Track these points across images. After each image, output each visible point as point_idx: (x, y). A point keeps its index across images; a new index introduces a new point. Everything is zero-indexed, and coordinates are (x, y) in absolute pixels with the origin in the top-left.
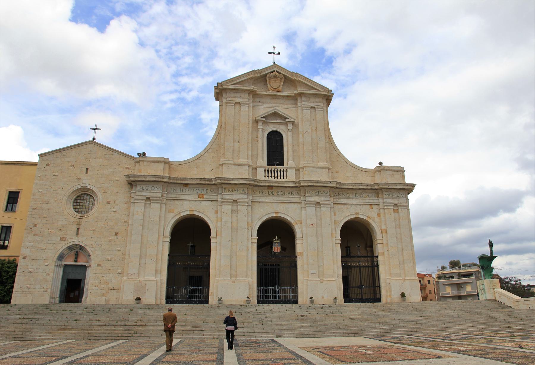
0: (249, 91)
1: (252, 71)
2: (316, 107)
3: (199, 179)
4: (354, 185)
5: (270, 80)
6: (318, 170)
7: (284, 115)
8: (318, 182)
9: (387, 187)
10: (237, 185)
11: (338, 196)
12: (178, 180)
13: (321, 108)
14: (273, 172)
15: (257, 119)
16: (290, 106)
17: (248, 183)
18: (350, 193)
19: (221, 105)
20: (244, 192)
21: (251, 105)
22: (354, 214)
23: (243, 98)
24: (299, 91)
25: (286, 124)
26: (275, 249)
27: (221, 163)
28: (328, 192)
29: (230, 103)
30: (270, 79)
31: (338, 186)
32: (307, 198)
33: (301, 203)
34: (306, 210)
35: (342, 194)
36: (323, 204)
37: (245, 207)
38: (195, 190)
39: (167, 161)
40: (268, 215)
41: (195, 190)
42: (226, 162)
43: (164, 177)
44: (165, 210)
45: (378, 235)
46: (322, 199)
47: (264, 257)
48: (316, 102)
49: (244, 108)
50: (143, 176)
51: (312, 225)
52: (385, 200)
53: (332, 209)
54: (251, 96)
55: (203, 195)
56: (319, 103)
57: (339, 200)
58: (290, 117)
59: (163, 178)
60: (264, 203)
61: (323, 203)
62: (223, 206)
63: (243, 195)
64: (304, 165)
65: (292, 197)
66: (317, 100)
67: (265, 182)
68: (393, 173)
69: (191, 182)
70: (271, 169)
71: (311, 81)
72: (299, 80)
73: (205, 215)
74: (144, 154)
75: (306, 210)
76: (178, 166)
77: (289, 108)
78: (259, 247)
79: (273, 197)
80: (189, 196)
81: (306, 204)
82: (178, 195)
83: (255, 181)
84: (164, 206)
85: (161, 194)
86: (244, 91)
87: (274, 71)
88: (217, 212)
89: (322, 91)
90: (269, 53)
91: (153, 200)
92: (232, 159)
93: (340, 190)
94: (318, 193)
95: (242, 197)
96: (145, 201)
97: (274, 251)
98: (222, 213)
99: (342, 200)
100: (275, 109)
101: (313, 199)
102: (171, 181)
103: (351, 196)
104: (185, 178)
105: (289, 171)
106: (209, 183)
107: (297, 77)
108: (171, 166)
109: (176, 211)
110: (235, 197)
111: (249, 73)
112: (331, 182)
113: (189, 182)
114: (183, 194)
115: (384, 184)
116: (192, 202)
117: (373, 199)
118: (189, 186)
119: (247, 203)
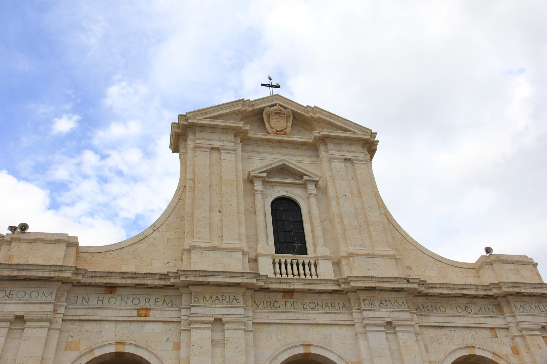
1: (239, 101)
3: (140, 276)
4: (451, 286)
5: (269, 118)
6: (378, 261)
7: (300, 170)
8: (385, 280)
9: (518, 290)
10: (222, 288)
11: (423, 311)
12: (95, 277)
13: (362, 161)
15: (251, 174)
16: (307, 159)
17: (245, 281)
19: (183, 163)
22: (463, 348)
23: (224, 141)
24: (322, 133)
25: (304, 186)
27: (186, 247)
28: (405, 303)
29: (201, 147)
30: (269, 115)
31: (422, 289)
32: (365, 314)
33: (353, 325)
34: (367, 339)
35: (430, 308)
36: (399, 326)
37: (240, 334)
38: (131, 299)
39: (74, 241)
40: (289, 351)
41: (131, 299)
42: (197, 244)
43: (63, 269)
44: (58, 345)
46: (396, 315)
48: (353, 152)
49: (226, 157)
50: (14, 267)
52: (519, 319)
53: (420, 337)
54: (239, 140)
55: (148, 310)
56: (358, 153)
57: (428, 318)
58: (311, 173)
59: (61, 271)
60: (278, 326)
61: (399, 323)
62: (193, 332)
63: (234, 307)
64: (349, 252)
65: (335, 313)
66: (354, 148)
67: (278, 281)
68: (519, 267)
69: (123, 281)
70: (286, 260)
71: (340, 119)
72: (319, 118)
73: (151, 352)
74: (24, 227)
75: (367, 339)
76: (95, 255)
79: (296, 313)
80: (117, 313)
81: (365, 326)
82: (91, 311)
83: (259, 278)
84: (55, 335)
85: (52, 306)
86: (225, 130)
88: (177, 346)
89: (360, 133)
90: (263, 85)
92: (208, 241)
93: (426, 298)
94: (385, 304)
95: (232, 311)
96: (11, 324)
98: (189, 347)
100: (283, 160)
101: (378, 314)
102: (80, 278)
103: (449, 311)
104: (112, 272)
105: (321, 263)
106: (162, 282)
107: (315, 113)
108: (81, 255)
109: (83, 347)
110: (218, 311)
112: (408, 280)
114: (103, 309)
115: (510, 285)
116: (124, 325)
117: (493, 317)
118: (119, 291)
119: (244, 323)
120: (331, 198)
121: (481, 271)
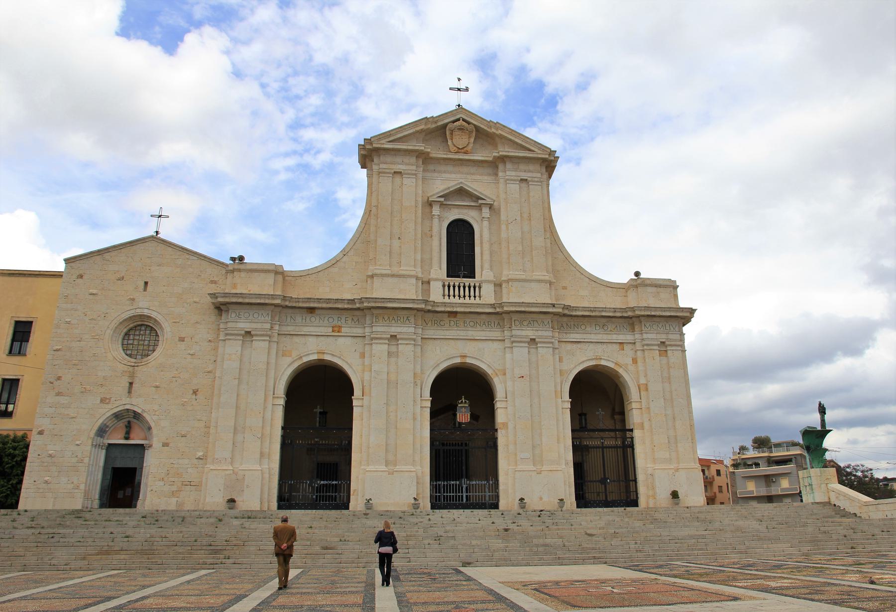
0: (417, 153)
1: (422, 119)
2: (529, 179)
3: (332, 301)
4: (592, 309)
5: (452, 134)
6: (533, 285)
7: (476, 193)
8: (533, 305)
9: (649, 313)
10: (398, 311)
11: (565, 329)
12: (298, 302)
13: (537, 182)
14: (457, 289)
15: (430, 199)
16: (486, 178)
17: (416, 306)
18: (586, 324)
19: (369, 176)
20: (408, 323)
21: (420, 176)
22: (592, 359)
23: (407, 164)
24: (501, 153)
25: (479, 208)
26: (461, 417)
27: (370, 274)
28: (550, 322)
29: (384, 173)
30: (452, 132)
31: (566, 312)
32: (514, 332)
33: (504, 340)
34: (512, 353)
35: (573, 326)
36: (540, 342)
37: (411, 348)
38: (326, 318)
39: (280, 270)
40: (449, 361)
41: (326, 318)
42: (378, 272)
43: (274, 297)
44: (277, 353)
45: (633, 394)
46: (540, 333)
47: (442, 431)
48: (530, 171)
49: (409, 182)
50: (239, 295)
51: (523, 377)
52: (645, 336)
53: (557, 351)
54: (420, 162)
55: (340, 327)
56: (534, 173)
57: (568, 335)
58: (486, 196)
59: (273, 298)
60: (442, 341)
61: (540, 340)
62: (374, 346)
63: (407, 327)
64: (510, 277)
65: (490, 331)
66: (531, 167)
67: (444, 305)
68: (659, 289)
69: (320, 305)
70: (454, 283)
71: (521, 136)
72: (501, 135)
73: (343, 360)
74: (241, 258)
75: (512, 353)
76: (297, 278)
77: (483, 181)
78: (434, 414)
79: (458, 330)
80: (317, 329)
81: (513, 342)
82: (297, 327)
83: (427, 303)
84: (274, 346)
85: (269, 325)
86: (408, 152)
87: (458, 120)
88: (363, 355)
89: (539, 152)
90: (451, 89)
91: (257, 335)
92: (388, 267)
93: (570, 318)
94: (532, 324)
95: (405, 330)
96: (243, 337)
97: (460, 420)
98: (371, 357)
99: (572, 336)
100: (461, 183)
101: (524, 333)
102: (287, 303)
103: (588, 329)
104: (310, 299)
105: (484, 286)
106: (350, 306)
107: (497, 129)
108: (287, 278)
109: (295, 354)
110: (394, 330)
111: (417, 123)
112: (554, 305)
113: (316, 305)
114: (307, 326)
115: (643, 309)
116: (322, 338)
117: (624, 334)
118: (317, 312)
119: (414, 340)
120: (502, 222)
121: (629, 292)
